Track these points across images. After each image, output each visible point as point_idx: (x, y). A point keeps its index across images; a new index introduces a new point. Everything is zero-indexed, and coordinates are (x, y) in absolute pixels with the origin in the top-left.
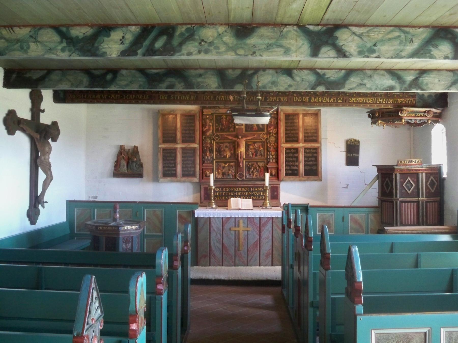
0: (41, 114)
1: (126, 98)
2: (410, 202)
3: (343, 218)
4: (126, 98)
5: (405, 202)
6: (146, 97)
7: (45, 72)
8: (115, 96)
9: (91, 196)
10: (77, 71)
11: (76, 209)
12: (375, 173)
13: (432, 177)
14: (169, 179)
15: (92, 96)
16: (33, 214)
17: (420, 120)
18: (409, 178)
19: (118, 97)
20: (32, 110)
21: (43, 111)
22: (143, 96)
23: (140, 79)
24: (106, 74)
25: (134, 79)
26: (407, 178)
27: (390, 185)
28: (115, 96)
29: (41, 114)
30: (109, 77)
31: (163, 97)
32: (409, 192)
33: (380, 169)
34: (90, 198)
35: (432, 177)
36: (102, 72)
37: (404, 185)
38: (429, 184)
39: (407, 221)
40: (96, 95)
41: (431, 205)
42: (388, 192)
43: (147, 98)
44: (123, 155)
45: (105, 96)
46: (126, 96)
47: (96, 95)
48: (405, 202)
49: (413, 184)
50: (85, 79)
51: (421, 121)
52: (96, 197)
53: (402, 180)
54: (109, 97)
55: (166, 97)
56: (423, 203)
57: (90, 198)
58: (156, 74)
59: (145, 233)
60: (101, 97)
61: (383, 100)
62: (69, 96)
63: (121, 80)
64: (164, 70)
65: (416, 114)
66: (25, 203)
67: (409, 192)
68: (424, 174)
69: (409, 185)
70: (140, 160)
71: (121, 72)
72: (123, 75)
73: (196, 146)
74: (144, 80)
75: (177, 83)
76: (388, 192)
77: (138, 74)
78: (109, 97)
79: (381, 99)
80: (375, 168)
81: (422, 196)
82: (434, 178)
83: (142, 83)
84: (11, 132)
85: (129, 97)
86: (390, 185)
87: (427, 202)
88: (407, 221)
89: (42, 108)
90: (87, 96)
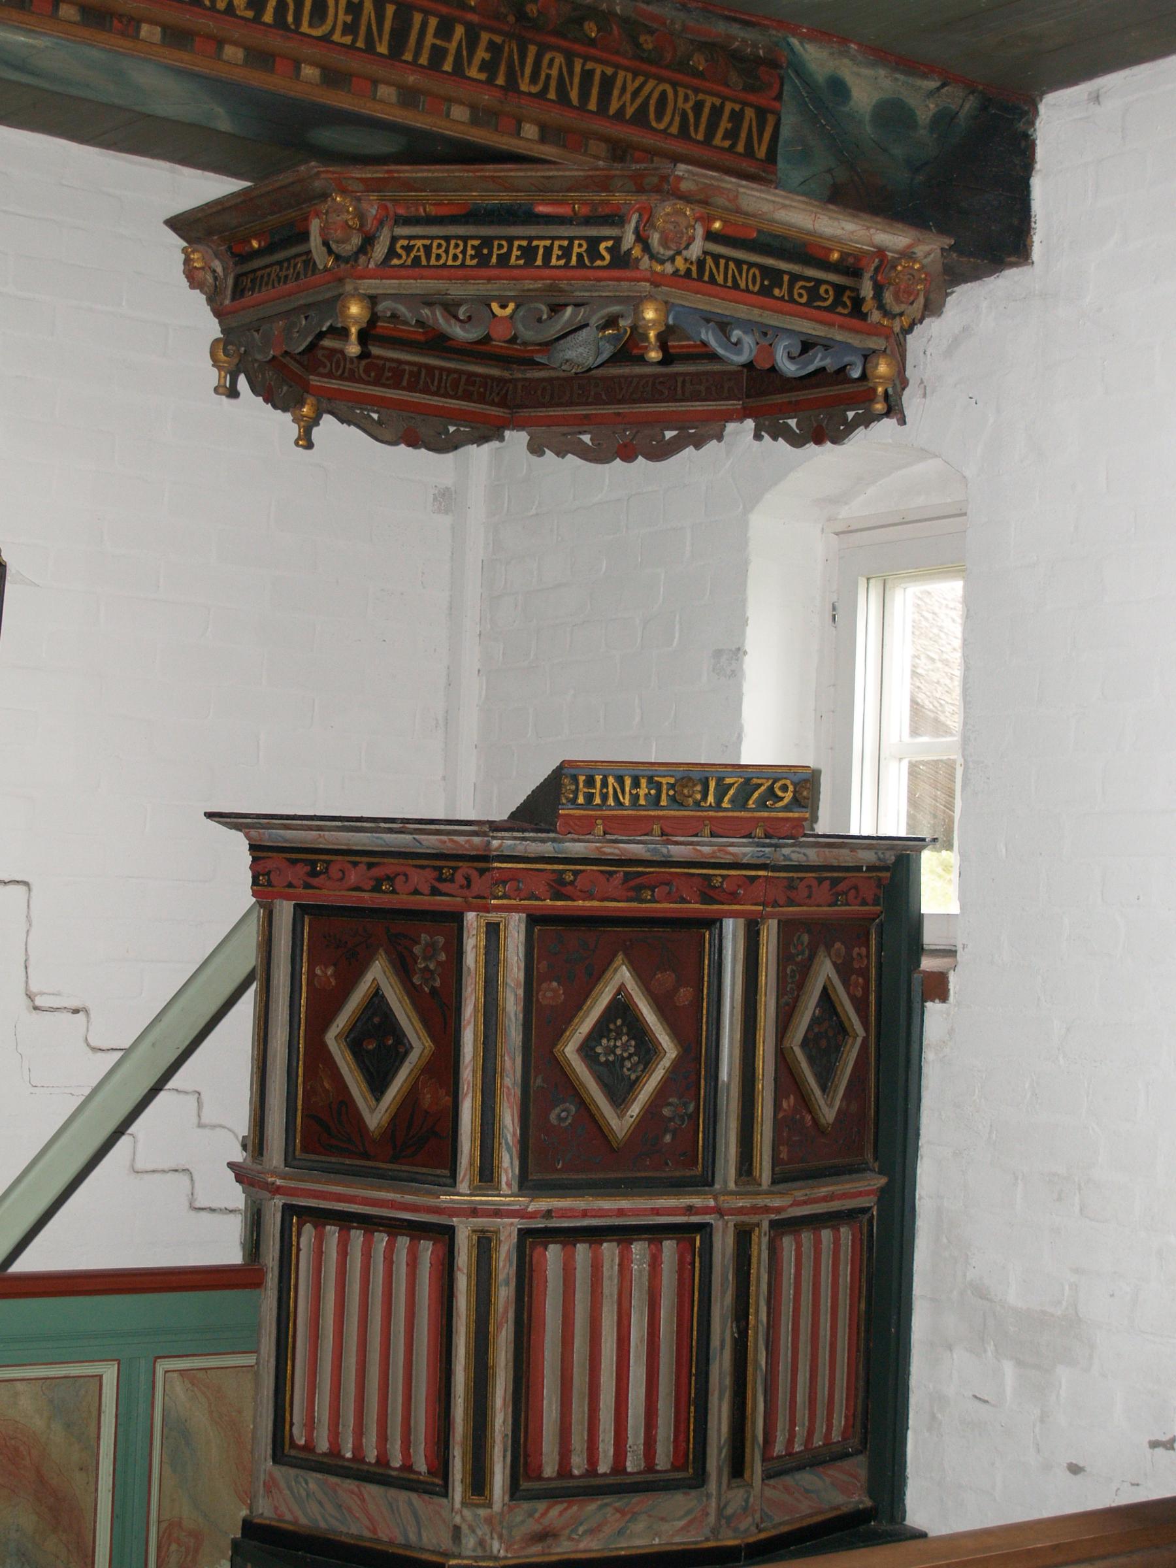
2: (624, 1234)
3: (1133, 1485)
5: (569, 1236)
12: (222, 889)
13: (825, 971)
14: (96, 54)
17: (807, 346)
18: (623, 975)
26: (596, 975)
27: (420, 1045)
32: (620, 1123)
33: (286, 857)
35: (825, 971)
37: (570, 1050)
38: (804, 1044)
39: (578, 1440)
41: (610, 1269)
42: (376, 1115)
48: (569, 1236)
49: (664, 1039)
51: (819, 360)
53: (552, 992)
56: (485, 1244)
61: (472, 40)
65: (774, 276)
67: (620, 1123)
68: (769, 934)
69: (623, 1044)
76: (376, 1115)
79: (445, 31)
80: (236, 849)
81: (487, 1175)
82: (844, 970)
86: (420, 1045)
87: (533, 1238)
88: (578, 1440)
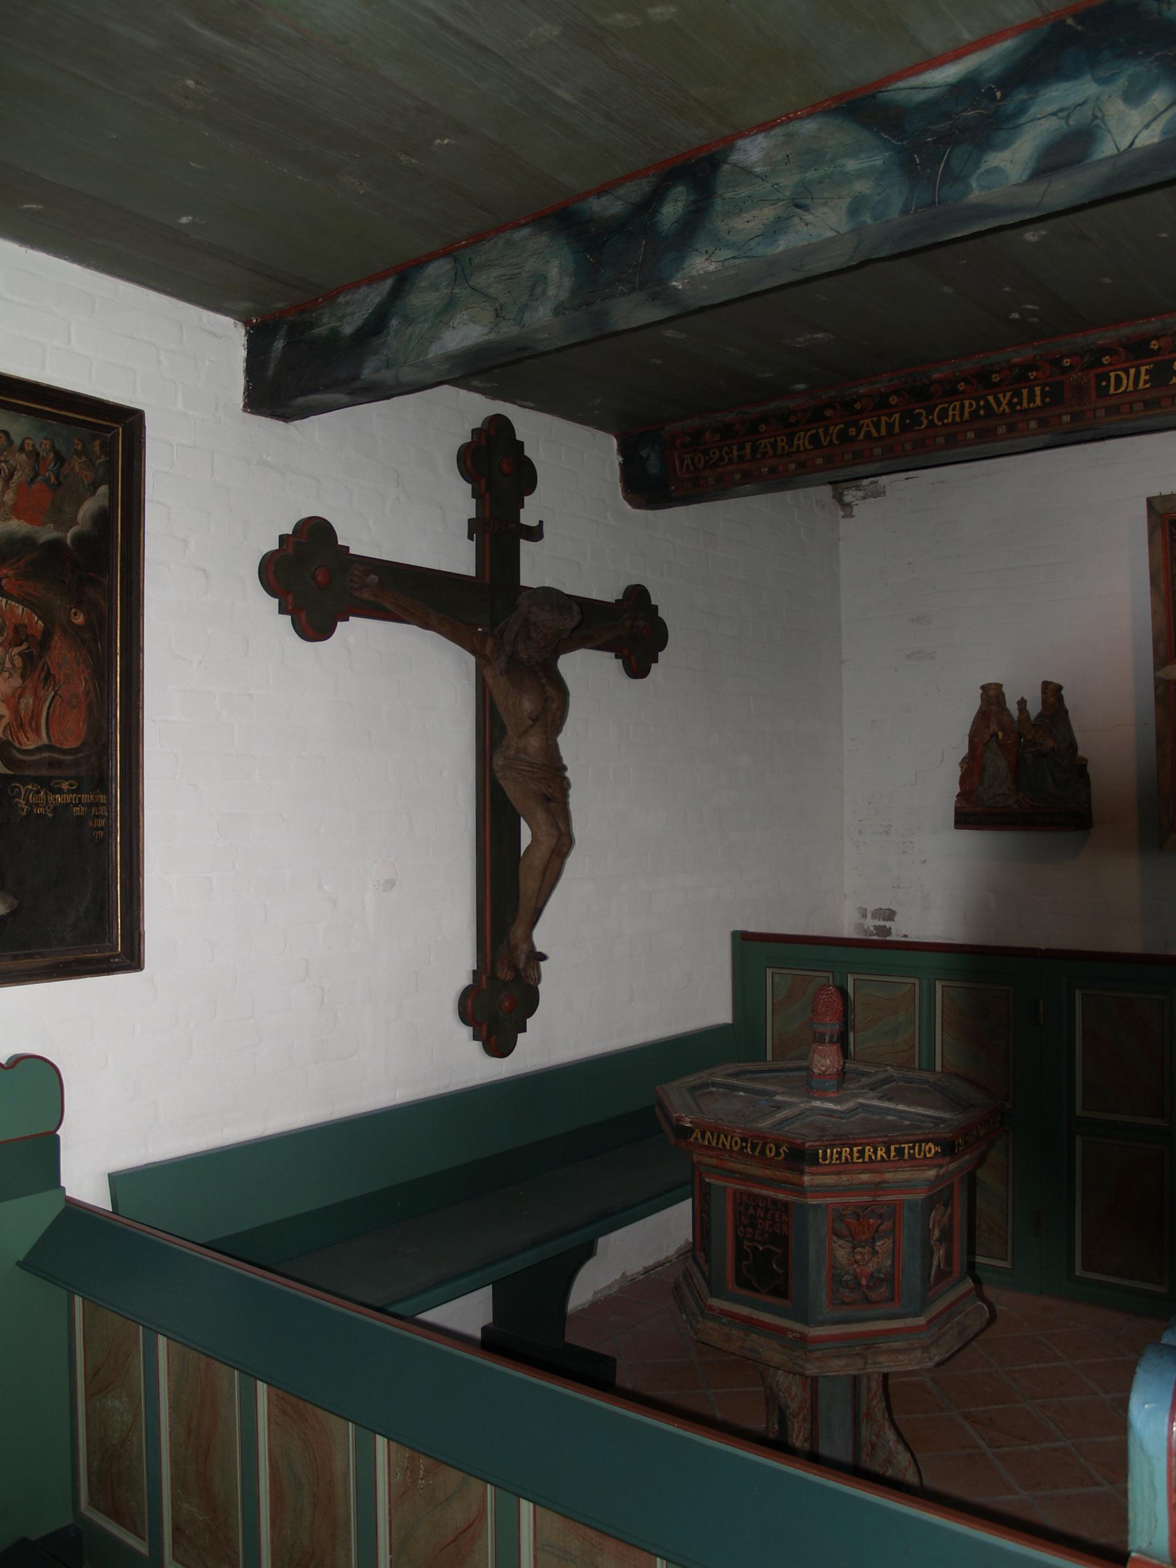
0: (524, 544)
1: (931, 424)
4: (931, 424)
6: (1032, 398)
7: (389, 282)
8: (877, 426)
9: (871, 908)
10: (518, 235)
11: (769, 972)
12: (968, 837)
15: (774, 445)
16: (499, 999)
19: (890, 426)
20: (475, 528)
21: (535, 534)
22: (1017, 394)
23: (851, 165)
24: (657, 197)
25: (811, 175)
28: (877, 426)
29: (524, 544)
30: (672, 210)
31: (1127, 384)
34: (864, 916)
36: (634, 191)
40: (790, 439)
43: (1038, 401)
44: (994, 727)
45: (834, 430)
46: (930, 412)
47: (790, 439)
50: (553, 267)
52: (890, 915)
54: (852, 431)
55: (1143, 377)
57: (864, 916)
58: (959, 89)
59: (1079, 1111)
60: (814, 440)
62: (682, 461)
63: (738, 209)
64: (1008, 44)
66: (450, 952)
70: (1073, 746)
71: (735, 157)
72: (747, 171)
73: (977, 193)
74: (878, 160)
75: (1115, 108)
77: (835, 135)
78: (852, 431)
83: (863, 187)
84: (314, 625)
85: (943, 414)
89: (528, 517)
90: (755, 449)
